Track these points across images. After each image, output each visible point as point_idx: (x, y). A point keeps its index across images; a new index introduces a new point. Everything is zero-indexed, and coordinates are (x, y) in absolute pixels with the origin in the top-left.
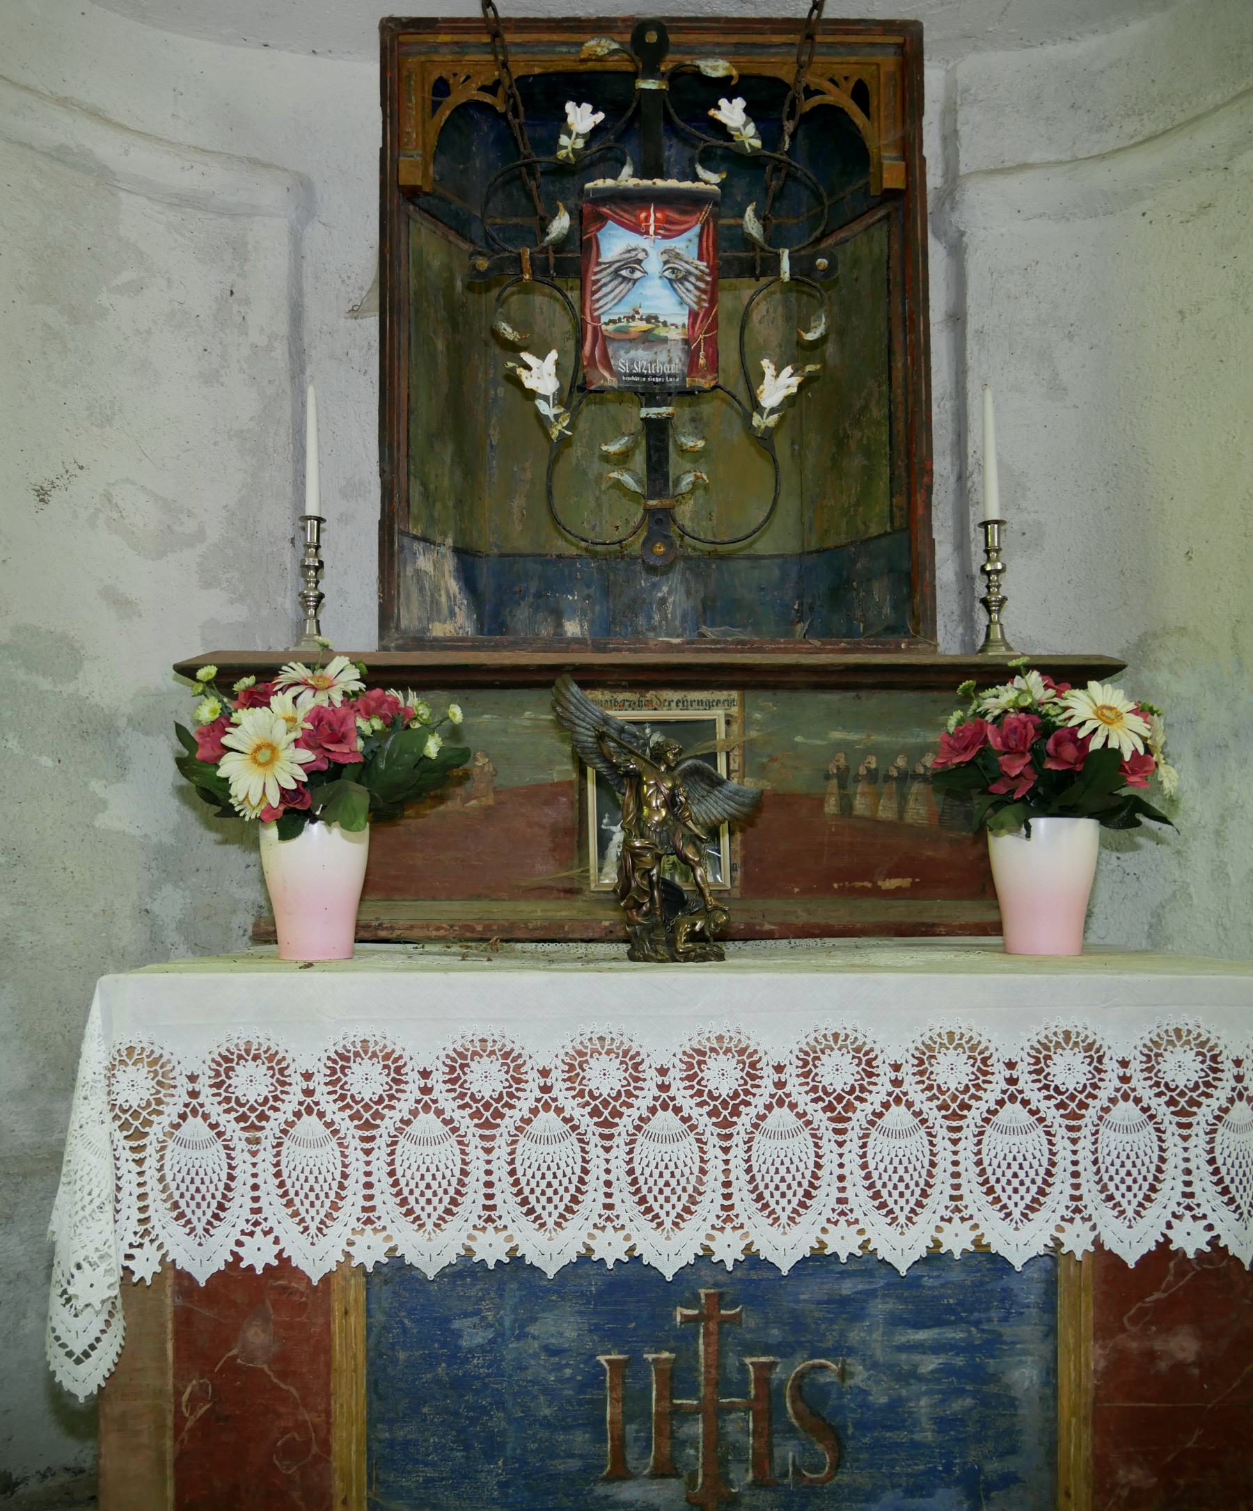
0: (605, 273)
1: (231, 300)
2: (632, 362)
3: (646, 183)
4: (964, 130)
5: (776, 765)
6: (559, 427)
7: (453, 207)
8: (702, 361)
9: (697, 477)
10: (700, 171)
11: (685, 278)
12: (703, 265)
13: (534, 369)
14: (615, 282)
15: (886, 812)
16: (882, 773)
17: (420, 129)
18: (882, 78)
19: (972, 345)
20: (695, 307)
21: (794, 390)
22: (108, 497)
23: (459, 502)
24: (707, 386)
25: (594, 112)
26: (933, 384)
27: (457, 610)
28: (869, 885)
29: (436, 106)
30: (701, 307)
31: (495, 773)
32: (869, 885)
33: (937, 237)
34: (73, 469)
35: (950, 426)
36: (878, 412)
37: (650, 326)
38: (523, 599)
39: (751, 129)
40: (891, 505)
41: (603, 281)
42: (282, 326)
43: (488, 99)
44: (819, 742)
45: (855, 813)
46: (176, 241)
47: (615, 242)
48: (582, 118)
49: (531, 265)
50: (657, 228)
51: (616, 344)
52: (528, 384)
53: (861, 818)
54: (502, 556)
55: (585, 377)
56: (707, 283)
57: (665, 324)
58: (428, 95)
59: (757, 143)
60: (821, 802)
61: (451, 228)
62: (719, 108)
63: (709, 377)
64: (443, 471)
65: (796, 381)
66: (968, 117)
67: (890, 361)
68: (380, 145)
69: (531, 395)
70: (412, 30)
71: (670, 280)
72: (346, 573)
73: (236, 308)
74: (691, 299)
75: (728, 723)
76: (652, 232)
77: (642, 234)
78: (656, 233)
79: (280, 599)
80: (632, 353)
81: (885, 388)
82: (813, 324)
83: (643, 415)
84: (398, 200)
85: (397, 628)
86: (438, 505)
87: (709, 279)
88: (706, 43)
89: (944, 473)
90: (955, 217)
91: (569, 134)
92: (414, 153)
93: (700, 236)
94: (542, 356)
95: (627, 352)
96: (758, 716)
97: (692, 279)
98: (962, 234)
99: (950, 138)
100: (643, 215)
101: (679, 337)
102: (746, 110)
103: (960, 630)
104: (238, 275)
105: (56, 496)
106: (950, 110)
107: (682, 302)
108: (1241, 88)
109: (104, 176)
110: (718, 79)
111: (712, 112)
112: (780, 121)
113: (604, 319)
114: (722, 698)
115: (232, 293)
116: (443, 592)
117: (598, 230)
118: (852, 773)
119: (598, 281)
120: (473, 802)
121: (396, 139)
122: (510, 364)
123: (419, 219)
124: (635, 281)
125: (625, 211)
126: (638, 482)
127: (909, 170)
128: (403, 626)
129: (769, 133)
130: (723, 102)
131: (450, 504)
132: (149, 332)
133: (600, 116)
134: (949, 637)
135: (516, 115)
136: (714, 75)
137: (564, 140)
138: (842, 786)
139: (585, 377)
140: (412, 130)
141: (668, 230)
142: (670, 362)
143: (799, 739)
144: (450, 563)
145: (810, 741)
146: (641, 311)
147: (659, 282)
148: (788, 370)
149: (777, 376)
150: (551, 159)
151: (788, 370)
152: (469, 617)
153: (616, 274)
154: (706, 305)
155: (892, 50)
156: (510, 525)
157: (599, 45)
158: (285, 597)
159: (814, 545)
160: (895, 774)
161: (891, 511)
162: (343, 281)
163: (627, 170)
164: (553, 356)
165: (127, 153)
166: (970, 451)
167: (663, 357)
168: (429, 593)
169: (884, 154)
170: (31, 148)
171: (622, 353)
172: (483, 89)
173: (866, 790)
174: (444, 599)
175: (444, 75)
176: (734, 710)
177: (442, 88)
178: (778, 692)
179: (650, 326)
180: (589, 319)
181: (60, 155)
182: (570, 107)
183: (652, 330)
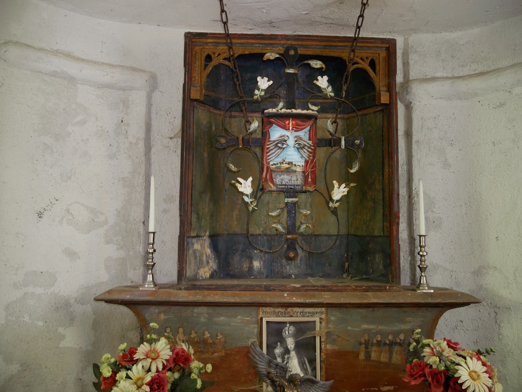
0: (272, 145)
1: (122, 124)
2: (282, 180)
3: (289, 111)
4: (411, 62)
5: (340, 339)
6: (252, 206)
7: (212, 98)
8: (310, 180)
9: (307, 226)
10: (310, 106)
11: (303, 147)
12: (310, 142)
13: (243, 184)
14: (276, 149)
15: (384, 358)
16: (383, 342)
17: (199, 76)
18: (381, 60)
19: (414, 147)
20: (307, 159)
21: (346, 193)
22: (68, 211)
23: (212, 216)
24: (311, 190)
25: (268, 81)
26: (400, 159)
27: (210, 260)
28: (377, 389)
29: (206, 66)
30: (310, 159)
31: (225, 342)
32: (377, 389)
33: (401, 101)
34: (54, 201)
35: (406, 176)
36: (378, 187)
37: (289, 166)
38: (237, 252)
39: (330, 89)
40: (383, 225)
41: (271, 148)
42: (142, 134)
43: (227, 63)
44: (357, 329)
45: (372, 359)
46: (100, 101)
47: (276, 133)
48: (264, 83)
49: (243, 142)
50: (293, 127)
51: (276, 173)
52: (240, 190)
53: (373, 361)
54: (228, 234)
55: (263, 186)
56: (312, 149)
57: (295, 165)
58: (203, 62)
59: (332, 94)
60: (357, 355)
61: (211, 106)
62: (317, 80)
63: (313, 186)
64: (205, 207)
65: (346, 190)
66: (413, 58)
67: (383, 168)
68: (183, 83)
69: (242, 194)
70: (197, 37)
71: (298, 148)
72: (165, 234)
73: (123, 127)
74: (306, 155)
75: (320, 323)
76: (291, 128)
77: (287, 130)
78: (292, 130)
79: (138, 247)
80: (282, 176)
81: (381, 177)
82: (353, 166)
83: (286, 201)
84: (189, 103)
85: (186, 277)
86: (203, 220)
87: (313, 148)
88: (313, 45)
89: (403, 194)
90: (408, 97)
91: (259, 89)
92: (197, 85)
93: (310, 131)
94: (246, 179)
95: (280, 176)
96: (333, 318)
97: (306, 148)
98: (411, 103)
99: (406, 64)
100: (287, 122)
101: (301, 170)
102: (328, 81)
103: (409, 258)
104: (125, 114)
105: (46, 214)
106: (406, 54)
107: (302, 157)
108: (515, 62)
109: (72, 80)
110: (317, 68)
111: (315, 82)
112: (341, 84)
113: (271, 163)
114: (319, 311)
115: (122, 121)
116: (204, 256)
117: (269, 128)
118: (371, 342)
119: (269, 148)
120: (216, 354)
121: (190, 80)
122: (233, 182)
123: (198, 106)
124: (284, 148)
125: (280, 120)
126: (284, 228)
127: (391, 97)
128: (187, 276)
129: (337, 90)
130: (319, 78)
131: (208, 218)
132: (88, 140)
133: (271, 82)
134: (405, 261)
135: (238, 80)
136: (316, 67)
137: (256, 92)
138: (366, 348)
139: (263, 186)
140: (196, 76)
141: (297, 128)
142: (297, 180)
143: (349, 328)
144: (207, 242)
145: (354, 329)
146: (286, 160)
147: (293, 149)
148: (344, 185)
149: (339, 188)
150: (251, 99)
151: (344, 185)
152: (214, 262)
153: (276, 145)
154: (312, 158)
155: (384, 49)
156: (234, 224)
157: (271, 55)
158: (140, 246)
159: (352, 232)
160: (388, 342)
161: (383, 228)
162: (167, 115)
163: (281, 105)
164: (250, 179)
165: (81, 71)
166: (414, 188)
167: (294, 178)
168: (198, 258)
169: (381, 89)
170: (42, 73)
171: (278, 176)
172: (225, 59)
173: (376, 349)
174: (204, 258)
175: (210, 53)
176: (323, 316)
177: (209, 58)
178: (341, 308)
179: (289, 166)
180: (265, 163)
181: (54, 74)
182: (259, 79)
183: (290, 167)
